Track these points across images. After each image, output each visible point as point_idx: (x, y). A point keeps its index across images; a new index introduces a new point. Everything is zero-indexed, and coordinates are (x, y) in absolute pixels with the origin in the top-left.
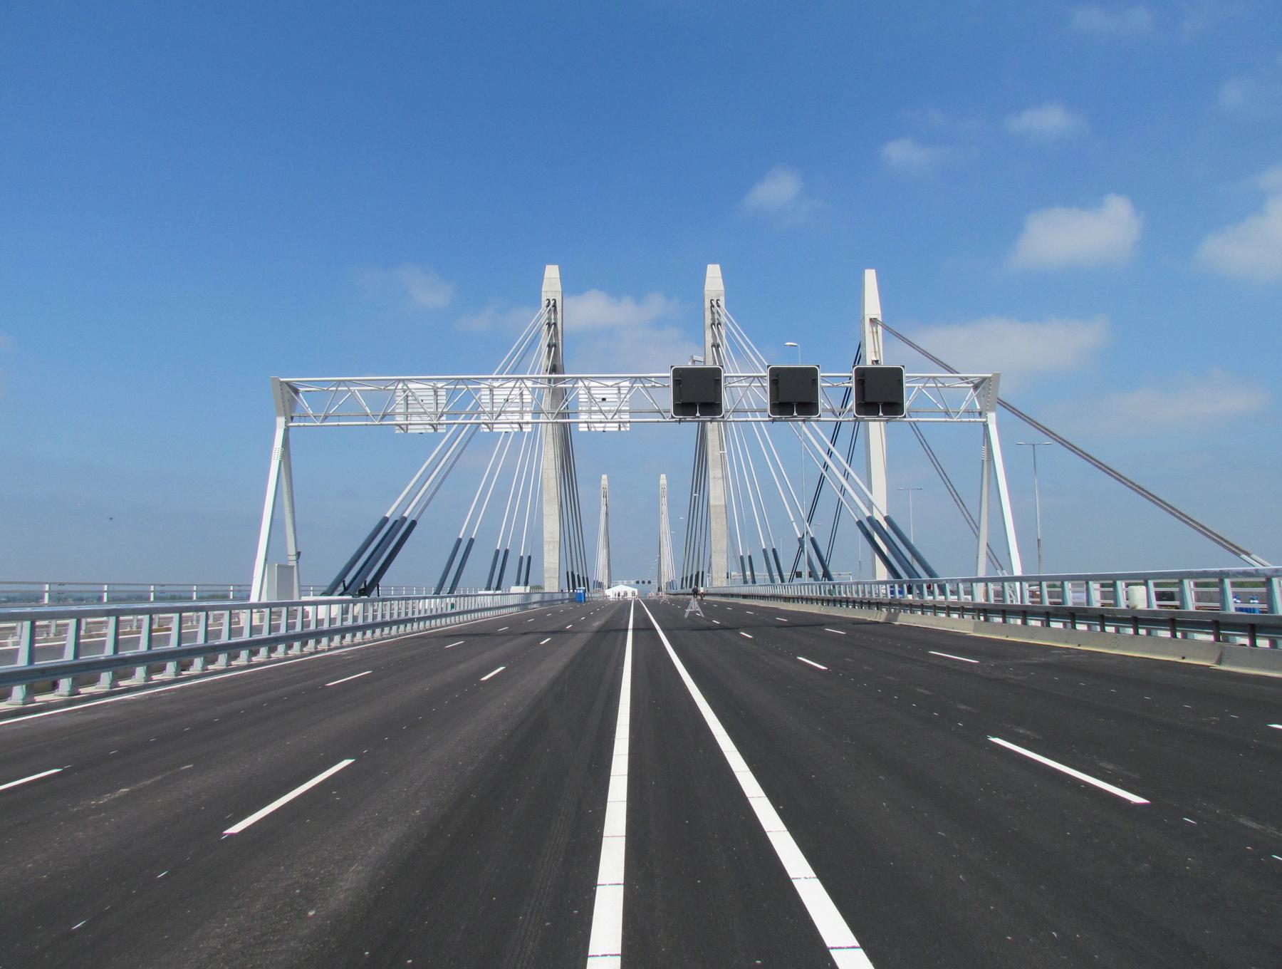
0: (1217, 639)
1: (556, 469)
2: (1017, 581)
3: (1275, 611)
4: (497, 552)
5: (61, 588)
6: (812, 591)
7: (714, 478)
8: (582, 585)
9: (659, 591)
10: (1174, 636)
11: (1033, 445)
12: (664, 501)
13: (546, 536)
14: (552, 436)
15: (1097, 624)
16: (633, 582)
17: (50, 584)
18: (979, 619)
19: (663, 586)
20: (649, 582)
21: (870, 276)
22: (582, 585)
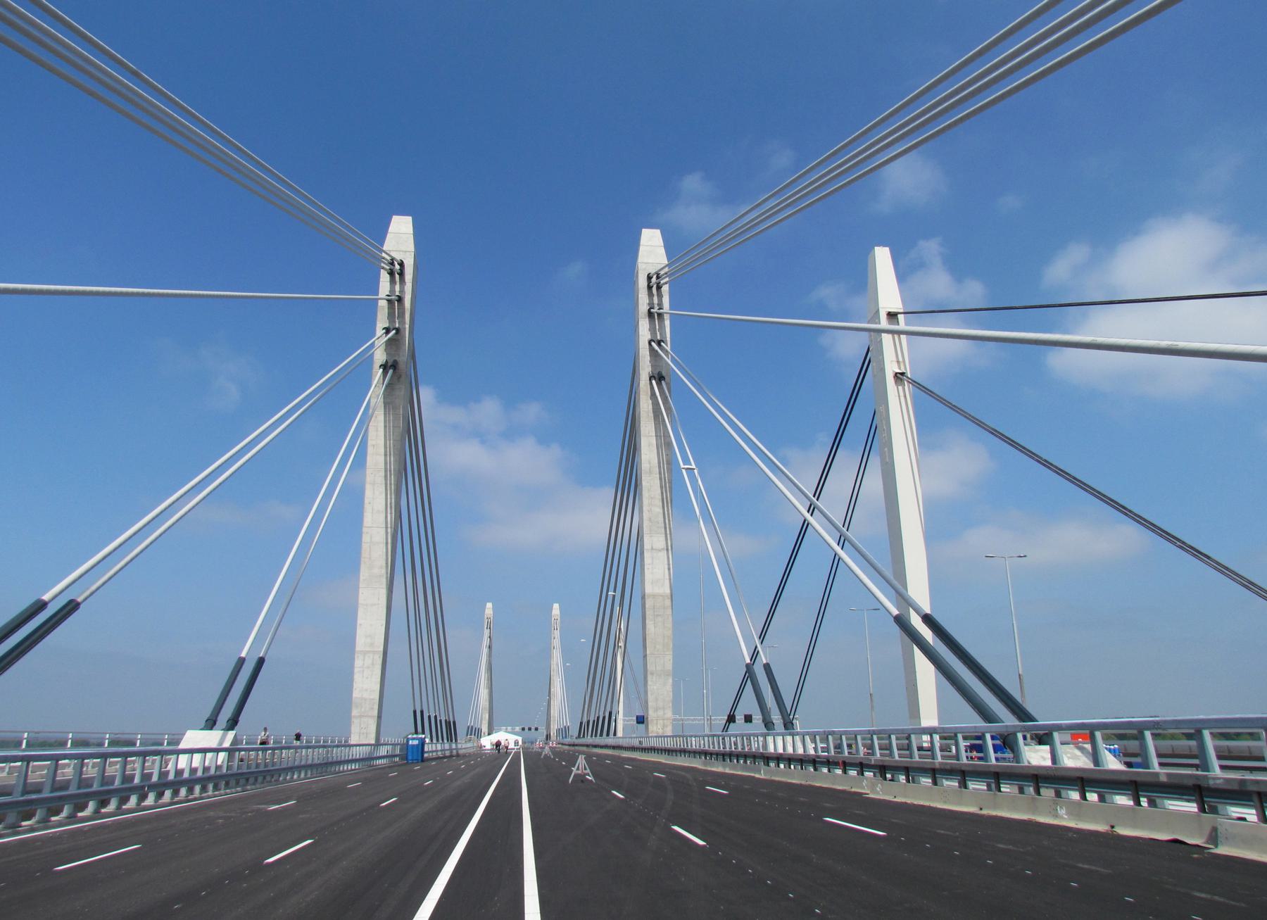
0: (1202, 810)
1: (387, 528)
2: (925, 733)
3: (1058, 762)
5: (37, 735)
6: (713, 744)
7: (652, 549)
8: (473, 733)
9: (547, 739)
10: (1138, 803)
12: (557, 634)
13: (361, 642)
14: (383, 474)
15: (1030, 786)
16: (518, 729)
17: (109, 734)
18: (790, 768)
19: (553, 733)
20: (536, 729)
22: (473, 733)
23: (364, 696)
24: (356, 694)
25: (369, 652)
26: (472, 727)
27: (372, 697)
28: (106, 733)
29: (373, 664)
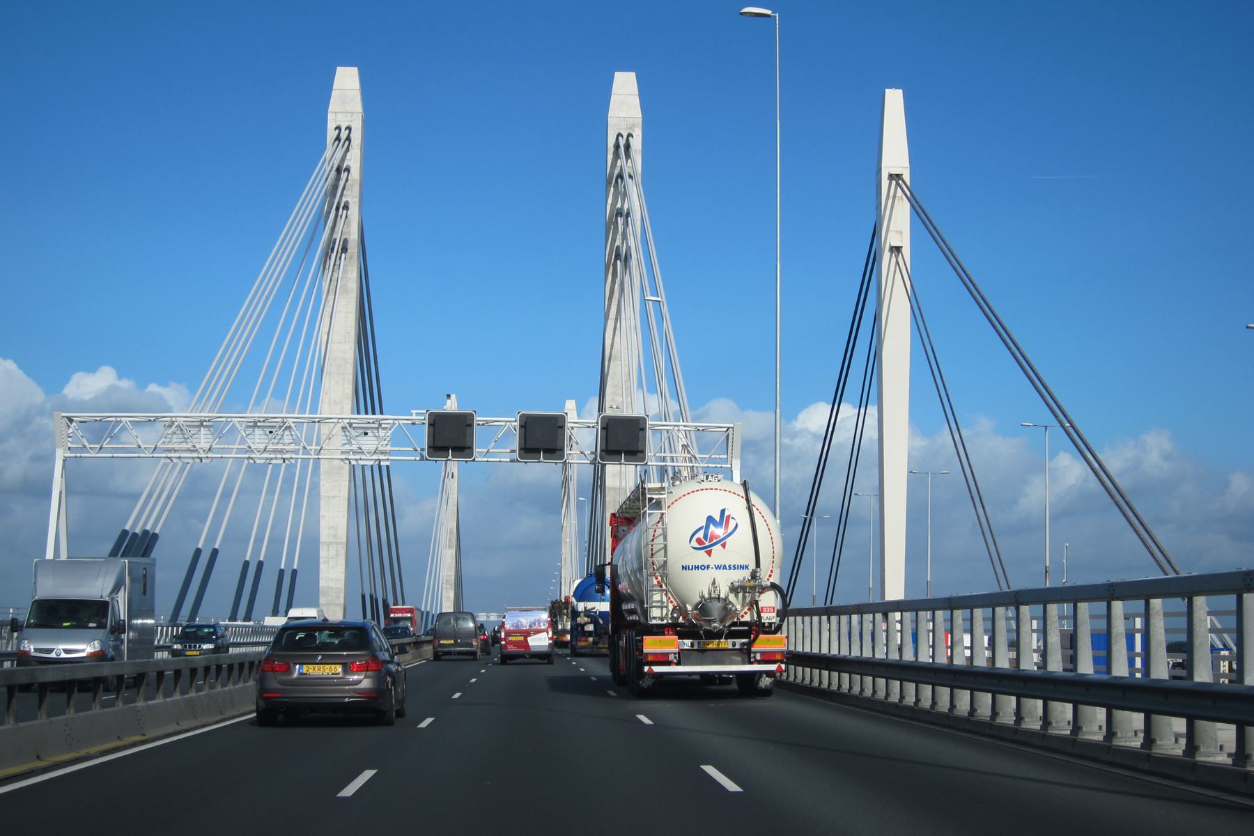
4: (246, 564)
11: (1046, 427)
21: (894, 100)
23: (331, 585)
24: (322, 583)
25: (331, 543)
26: (428, 613)
27: (338, 586)
28: (10, 608)
29: (337, 555)
